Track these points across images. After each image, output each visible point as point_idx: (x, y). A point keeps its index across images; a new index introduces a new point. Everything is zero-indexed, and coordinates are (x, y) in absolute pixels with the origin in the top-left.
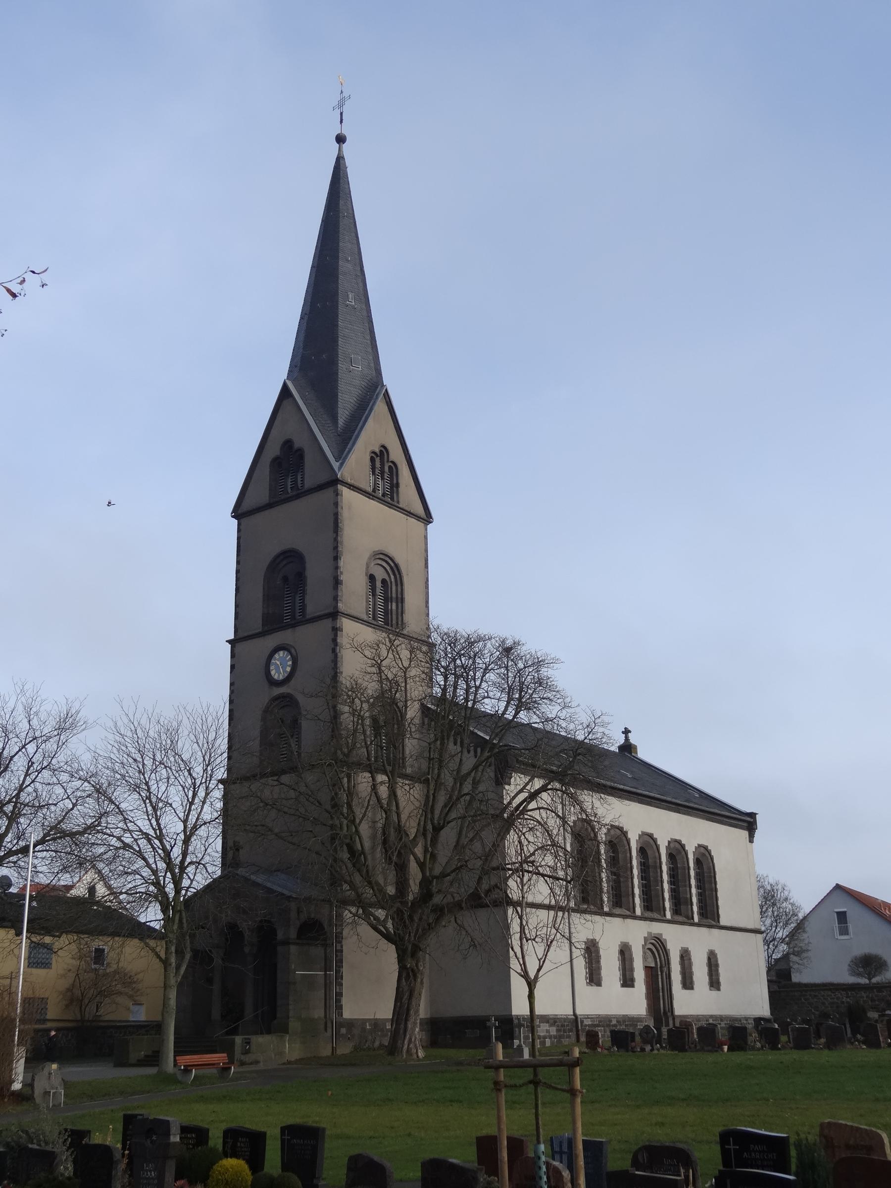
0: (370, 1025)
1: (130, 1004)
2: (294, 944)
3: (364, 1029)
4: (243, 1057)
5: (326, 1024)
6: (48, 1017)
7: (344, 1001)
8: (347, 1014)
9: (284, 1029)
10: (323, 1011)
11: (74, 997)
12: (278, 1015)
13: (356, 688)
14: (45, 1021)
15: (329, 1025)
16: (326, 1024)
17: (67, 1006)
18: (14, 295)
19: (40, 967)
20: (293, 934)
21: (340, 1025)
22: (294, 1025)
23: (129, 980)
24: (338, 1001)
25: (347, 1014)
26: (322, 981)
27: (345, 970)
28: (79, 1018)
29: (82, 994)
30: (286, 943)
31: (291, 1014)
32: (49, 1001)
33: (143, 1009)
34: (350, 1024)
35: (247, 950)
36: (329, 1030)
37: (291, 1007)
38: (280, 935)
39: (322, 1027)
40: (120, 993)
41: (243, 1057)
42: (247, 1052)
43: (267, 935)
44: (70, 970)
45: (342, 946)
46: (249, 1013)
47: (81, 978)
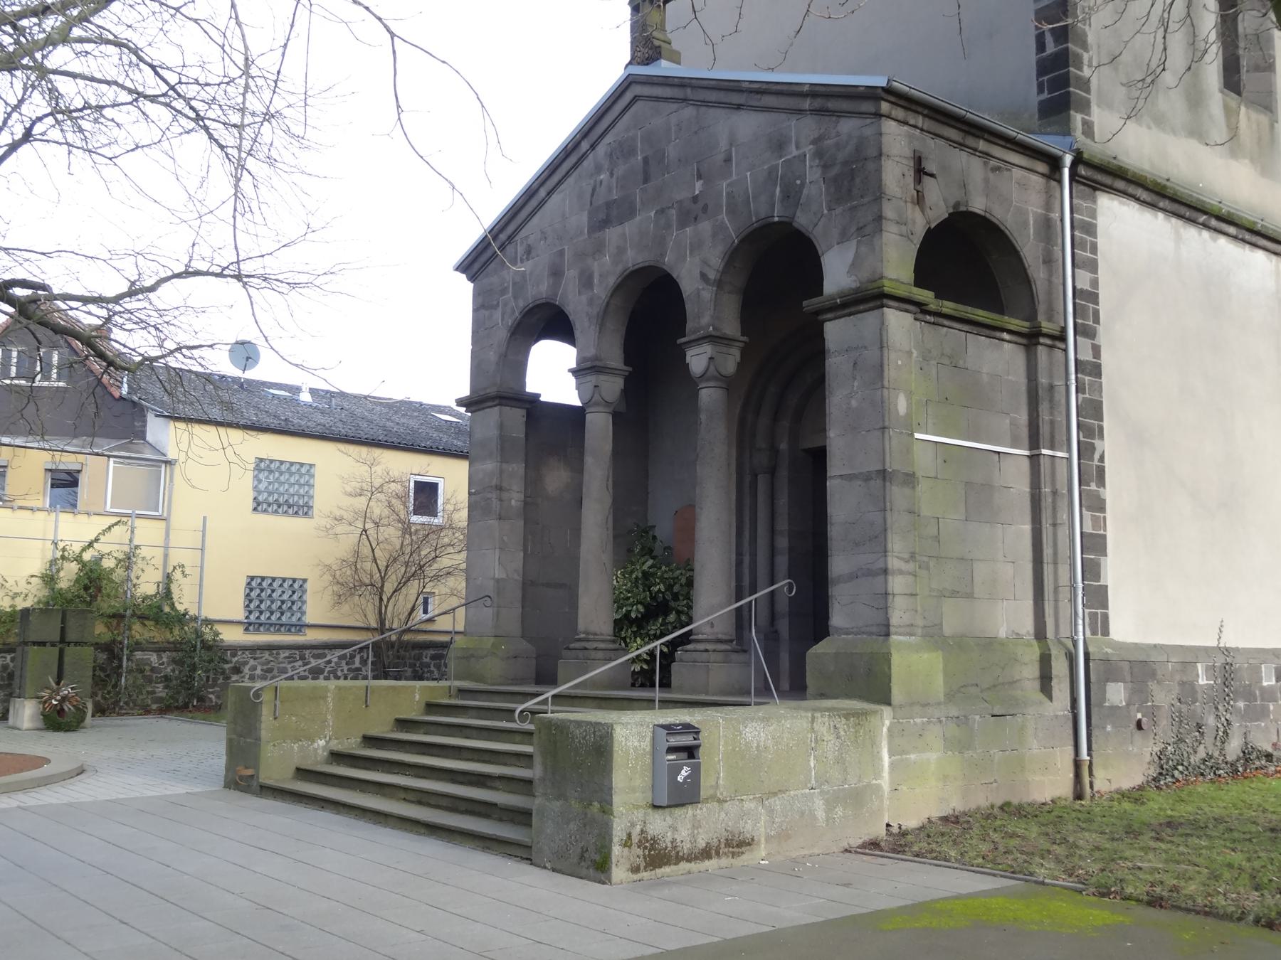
0: (1210, 670)
2: (904, 302)
3: (1188, 691)
4: (659, 825)
5: (1045, 661)
6: (308, 619)
7: (1113, 571)
8: (1129, 625)
9: (870, 683)
10: (1028, 604)
11: (356, 581)
12: (837, 619)
13: (854, 266)
14: (301, 627)
15: (1059, 667)
16: (1045, 661)
20: (897, 263)
21: (1105, 668)
22: (913, 664)
24: (1092, 570)
25: (1129, 625)
26: (1022, 486)
27: (1111, 446)
30: (870, 298)
31: (897, 617)
32: (308, 586)
34: (1141, 667)
35: (697, 360)
36: (1060, 689)
37: (897, 584)
38: (838, 273)
39: (1030, 672)
41: (659, 825)
42: (683, 796)
43: (777, 267)
45: (1096, 351)
46: (712, 608)
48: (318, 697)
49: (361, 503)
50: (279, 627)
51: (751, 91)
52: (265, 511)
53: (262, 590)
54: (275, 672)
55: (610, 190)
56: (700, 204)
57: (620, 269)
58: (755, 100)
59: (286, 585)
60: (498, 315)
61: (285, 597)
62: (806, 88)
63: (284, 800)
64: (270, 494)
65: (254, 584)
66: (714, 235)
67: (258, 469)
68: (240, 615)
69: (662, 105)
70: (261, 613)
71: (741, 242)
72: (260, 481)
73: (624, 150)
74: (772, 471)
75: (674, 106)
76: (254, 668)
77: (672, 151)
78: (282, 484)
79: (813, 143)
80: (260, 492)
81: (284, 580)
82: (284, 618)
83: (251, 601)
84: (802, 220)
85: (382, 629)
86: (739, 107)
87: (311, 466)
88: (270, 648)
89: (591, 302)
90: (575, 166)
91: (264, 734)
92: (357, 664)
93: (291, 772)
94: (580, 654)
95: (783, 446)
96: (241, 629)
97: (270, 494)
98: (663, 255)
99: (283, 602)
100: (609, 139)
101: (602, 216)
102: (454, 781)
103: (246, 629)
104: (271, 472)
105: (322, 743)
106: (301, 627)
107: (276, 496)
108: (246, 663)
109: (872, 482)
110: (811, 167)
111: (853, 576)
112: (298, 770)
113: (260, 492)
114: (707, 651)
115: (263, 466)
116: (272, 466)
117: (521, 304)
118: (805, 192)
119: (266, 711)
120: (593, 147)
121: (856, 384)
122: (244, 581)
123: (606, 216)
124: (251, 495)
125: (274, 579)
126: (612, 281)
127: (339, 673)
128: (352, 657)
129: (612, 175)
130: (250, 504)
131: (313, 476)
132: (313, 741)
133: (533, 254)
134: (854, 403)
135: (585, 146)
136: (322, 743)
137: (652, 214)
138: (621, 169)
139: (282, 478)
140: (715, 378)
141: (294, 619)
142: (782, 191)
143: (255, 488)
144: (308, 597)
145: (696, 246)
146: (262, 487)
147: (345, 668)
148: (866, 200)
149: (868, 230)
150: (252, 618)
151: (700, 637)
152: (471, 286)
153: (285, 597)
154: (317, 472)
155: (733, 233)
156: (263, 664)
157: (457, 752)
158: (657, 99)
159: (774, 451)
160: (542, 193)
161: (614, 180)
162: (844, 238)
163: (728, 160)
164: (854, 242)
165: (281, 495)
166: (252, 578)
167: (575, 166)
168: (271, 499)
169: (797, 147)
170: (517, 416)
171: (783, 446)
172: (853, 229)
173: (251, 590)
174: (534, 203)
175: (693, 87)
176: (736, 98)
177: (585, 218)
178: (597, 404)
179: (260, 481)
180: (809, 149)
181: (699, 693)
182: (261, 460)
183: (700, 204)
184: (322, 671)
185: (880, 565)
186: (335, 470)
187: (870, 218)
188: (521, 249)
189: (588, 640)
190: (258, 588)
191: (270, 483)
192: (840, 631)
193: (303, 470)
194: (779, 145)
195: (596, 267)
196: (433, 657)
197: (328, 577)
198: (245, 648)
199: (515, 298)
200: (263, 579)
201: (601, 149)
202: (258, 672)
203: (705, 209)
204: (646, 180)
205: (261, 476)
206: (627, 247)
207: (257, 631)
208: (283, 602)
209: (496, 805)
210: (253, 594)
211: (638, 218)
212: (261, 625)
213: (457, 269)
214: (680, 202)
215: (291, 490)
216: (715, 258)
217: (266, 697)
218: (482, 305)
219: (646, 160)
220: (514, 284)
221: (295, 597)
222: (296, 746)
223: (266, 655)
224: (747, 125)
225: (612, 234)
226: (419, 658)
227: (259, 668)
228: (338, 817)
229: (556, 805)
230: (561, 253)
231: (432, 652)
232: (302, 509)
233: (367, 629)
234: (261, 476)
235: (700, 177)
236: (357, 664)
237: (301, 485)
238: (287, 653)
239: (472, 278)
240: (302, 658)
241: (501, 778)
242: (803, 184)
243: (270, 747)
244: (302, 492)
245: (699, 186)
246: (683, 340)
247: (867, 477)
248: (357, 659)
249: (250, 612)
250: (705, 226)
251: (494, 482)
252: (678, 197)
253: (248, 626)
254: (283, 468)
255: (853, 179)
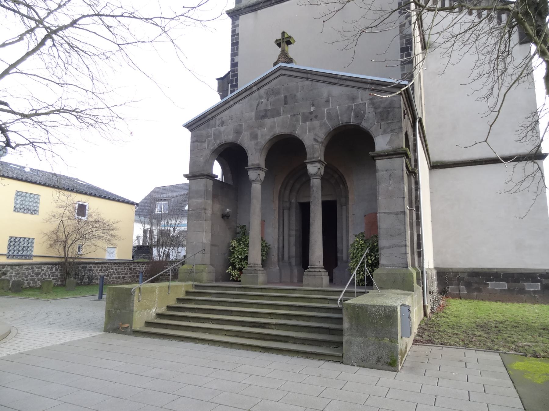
1: (106, 246)
6: (34, 253)
11: (58, 239)
13: (390, 142)
17: (51, 245)
18: (184, 7)
19: (27, 213)
23: (108, 228)
28: (63, 255)
29: (66, 237)
32: (35, 241)
33: (116, 251)
40: (99, 237)
44: (54, 216)
47: (65, 224)
48: (153, 291)
49: (61, 210)
50: (22, 257)
51: (341, 79)
52: (19, 211)
53: (15, 242)
54: (21, 274)
55: (267, 105)
56: (314, 115)
57: (272, 133)
58: (342, 82)
59: (26, 240)
60: (205, 145)
61: (25, 245)
62: (370, 81)
63: (151, 337)
64: (21, 205)
65: (12, 240)
66: (321, 126)
67: (17, 195)
68: (6, 252)
69: (294, 79)
70: (14, 251)
71: (333, 130)
72: (17, 200)
73: (275, 92)
74: (289, 209)
75: (301, 80)
76: (12, 273)
77: (299, 95)
78: (26, 201)
79: (369, 99)
80: (17, 204)
81: (25, 238)
82: (24, 253)
83: (10, 246)
84: (364, 125)
85: (66, 258)
86: (333, 84)
87: (39, 195)
88: (19, 265)
89: (257, 144)
90: (249, 95)
91: (135, 309)
92: (54, 271)
93: (143, 324)
94: (253, 272)
95: (293, 201)
96: (5, 257)
97: (21, 205)
98: (295, 130)
99: (24, 247)
100: (265, 87)
101: (262, 114)
102: (319, 333)
103: (8, 257)
104: (22, 196)
105: (154, 310)
106: (30, 257)
107: (24, 206)
108: (9, 271)
109: (399, 215)
110: (368, 108)
111: (389, 247)
112: (146, 322)
113: (17, 204)
114: (320, 271)
115: (19, 194)
116: (23, 194)
117: (218, 142)
118: (366, 116)
119: (136, 298)
120: (258, 89)
121: (391, 182)
122: (8, 238)
123: (263, 115)
124: (13, 205)
125: (21, 238)
126: (268, 138)
127: (47, 274)
128: (52, 268)
129: (268, 100)
130: (13, 209)
131: (39, 199)
132: (151, 310)
133: (225, 124)
134: (390, 188)
135: (255, 88)
136: (154, 310)
137: (289, 116)
138: (272, 99)
139: (27, 199)
140: (319, 176)
141: (28, 254)
142: (354, 114)
143: (15, 203)
144: (34, 245)
145: (311, 129)
146: (18, 202)
147: (49, 272)
148: (395, 121)
149: (396, 131)
150: (11, 253)
151: (315, 266)
152: (190, 133)
153: (25, 245)
154: (42, 198)
155: (330, 126)
156: (15, 271)
157: (231, 313)
158: (292, 76)
159: (290, 203)
160: (232, 103)
161: (269, 102)
162: (385, 132)
163: (328, 101)
164: (390, 135)
165: (25, 206)
166: (12, 237)
167: (249, 95)
168: (21, 207)
169: (362, 100)
170: (210, 182)
171: (293, 201)
172: (389, 130)
173: (11, 242)
174: (227, 106)
175: (311, 74)
176: (333, 80)
177: (253, 114)
178: (258, 181)
179: (17, 200)
180: (368, 102)
181: (318, 287)
182: (18, 192)
183: (314, 115)
184: (40, 274)
185: (403, 243)
186: (49, 200)
187: (397, 127)
188: (218, 122)
189: (255, 267)
190: (14, 242)
191: (21, 201)
192: (383, 265)
193: (35, 197)
194: (353, 99)
195: (259, 132)
196: (83, 268)
197: (46, 237)
198: (9, 265)
199: (215, 139)
200: (16, 238)
201: (262, 91)
202: (14, 274)
203: (316, 117)
204: (286, 103)
205: (18, 198)
206: (276, 126)
207: (12, 258)
208: (24, 247)
209: (294, 337)
210: (12, 244)
211: (281, 117)
212: (14, 256)
213: (185, 126)
214: (303, 113)
215: (30, 204)
216: (322, 135)
217: (137, 292)
218: (196, 142)
219: (285, 97)
220: (214, 134)
221: (29, 245)
222: (145, 313)
223: (17, 268)
224: (336, 90)
225: (268, 122)
226: (78, 267)
227: (14, 273)
228: (227, 349)
229: (359, 340)
230: (241, 125)
231: (83, 266)
232: (34, 211)
233: (60, 257)
234: (18, 198)
235: (313, 105)
236: (54, 271)
237: (34, 203)
238: (26, 267)
239: (191, 131)
240: (32, 268)
241: (276, 324)
242: (364, 113)
243: (137, 314)
244: (34, 205)
245: (312, 109)
246: (307, 161)
247: (397, 214)
248: (54, 269)
249: (10, 251)
250: (316, 123)
251: (203, 206)
252: (302, 111)
253: (8, 256)
254: (27, 195)
255: (389, 113)
